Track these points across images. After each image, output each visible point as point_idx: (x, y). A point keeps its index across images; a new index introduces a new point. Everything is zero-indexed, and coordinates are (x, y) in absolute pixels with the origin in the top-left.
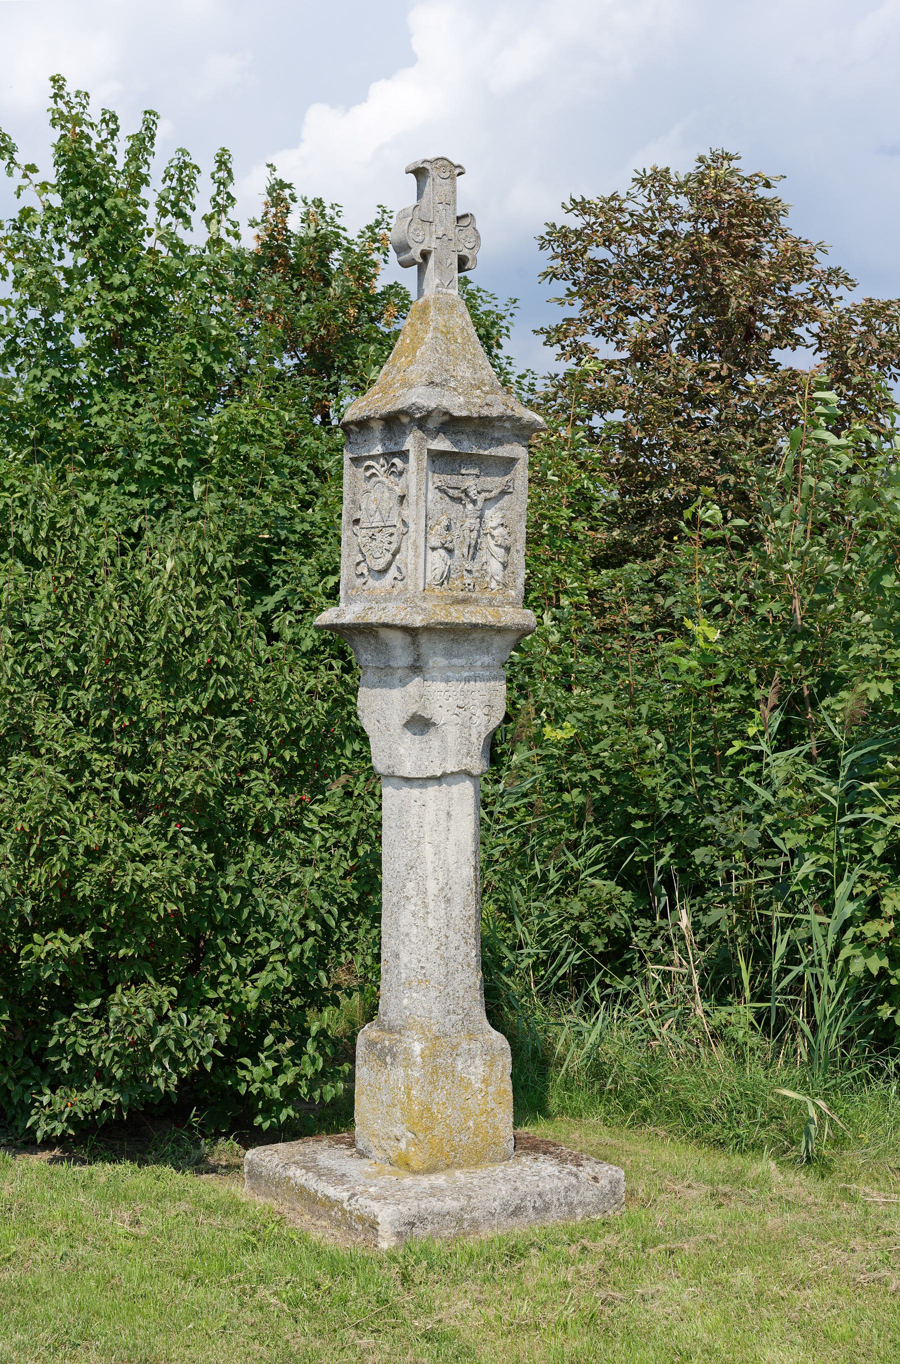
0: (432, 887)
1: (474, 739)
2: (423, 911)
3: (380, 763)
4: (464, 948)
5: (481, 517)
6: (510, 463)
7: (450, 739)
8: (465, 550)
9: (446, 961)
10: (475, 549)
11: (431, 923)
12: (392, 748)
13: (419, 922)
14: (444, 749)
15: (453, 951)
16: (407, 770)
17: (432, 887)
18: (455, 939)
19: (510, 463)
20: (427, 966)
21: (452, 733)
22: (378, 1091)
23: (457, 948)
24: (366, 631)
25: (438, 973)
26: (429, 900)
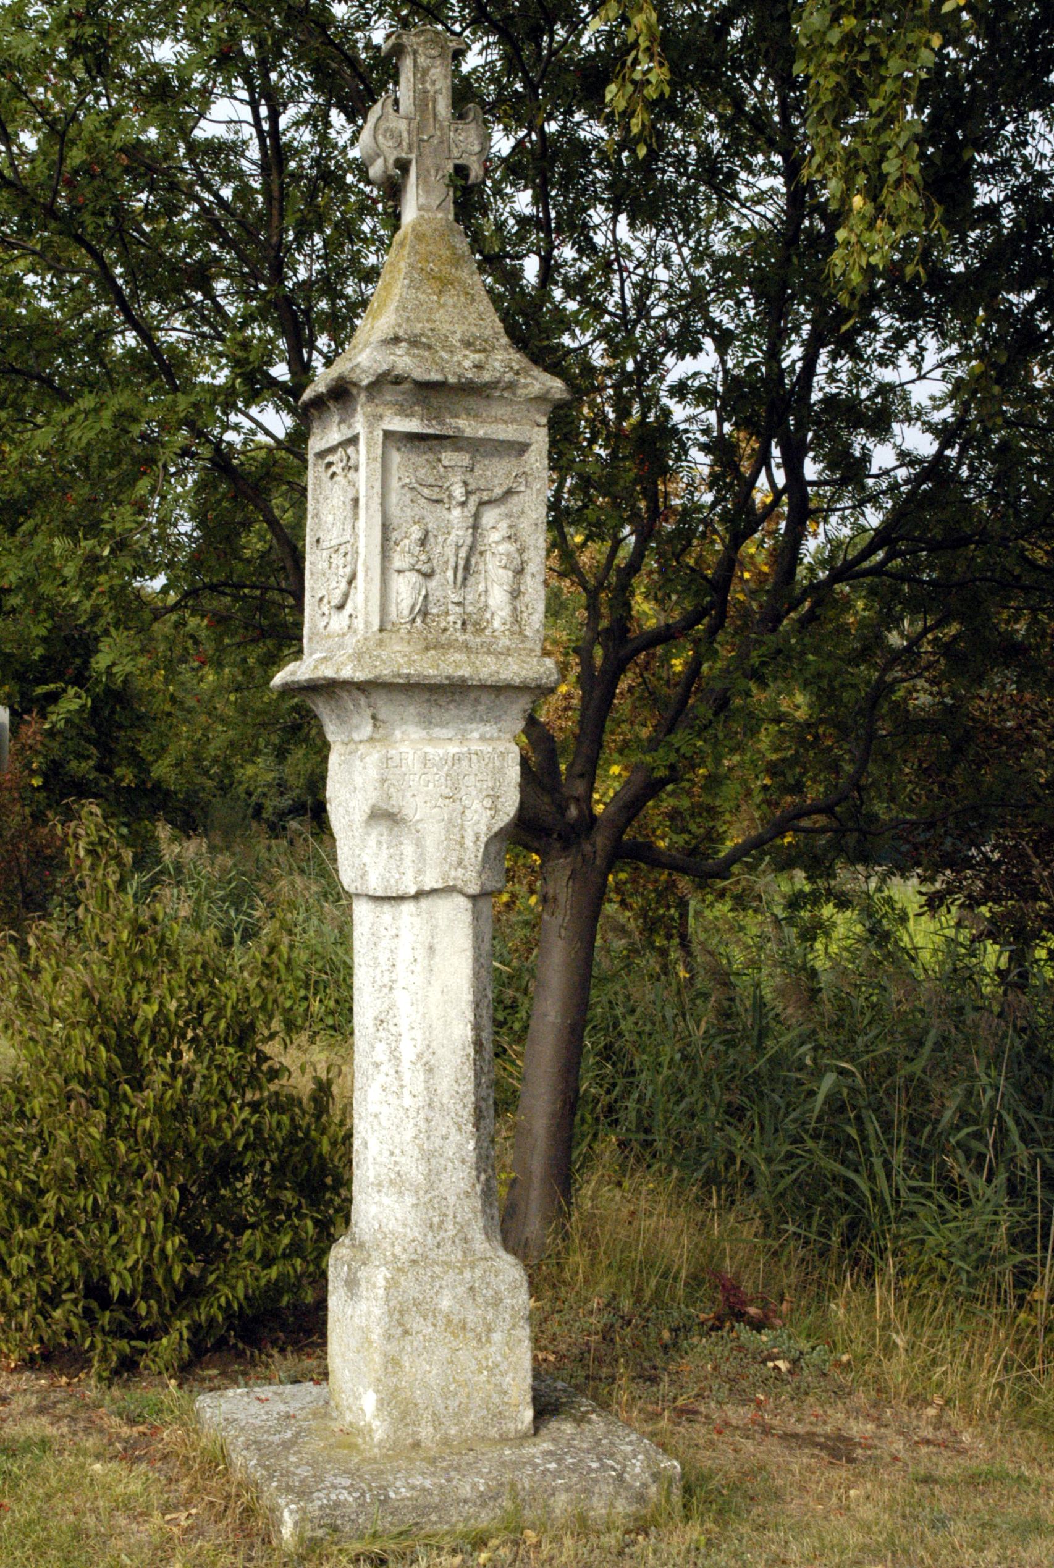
0: (408, 1052)
1: (469, 842)
2: (396, 1083)
3: (347, 877)
4: (455, 1137)
5: (475, 527)
6: (521, 448)
7: (430, 843)
8: (450, 574)
9: (428, 1156)
10: (467, 571)
11: (408, 1101)
12: (360, 856)
13: (392, 1099)
14: (421, 857)
15: (438, 1142)
16: (374, 886)
17: (408, 1052)
18: (444, 1125)
19: (521, 448)
20: (402, 1160)
21: (433, 833)
22: (355, 1316)
23: (445, 1138)
24: (328, 688)
25: (414, 1171)
26: (405, 1065)
